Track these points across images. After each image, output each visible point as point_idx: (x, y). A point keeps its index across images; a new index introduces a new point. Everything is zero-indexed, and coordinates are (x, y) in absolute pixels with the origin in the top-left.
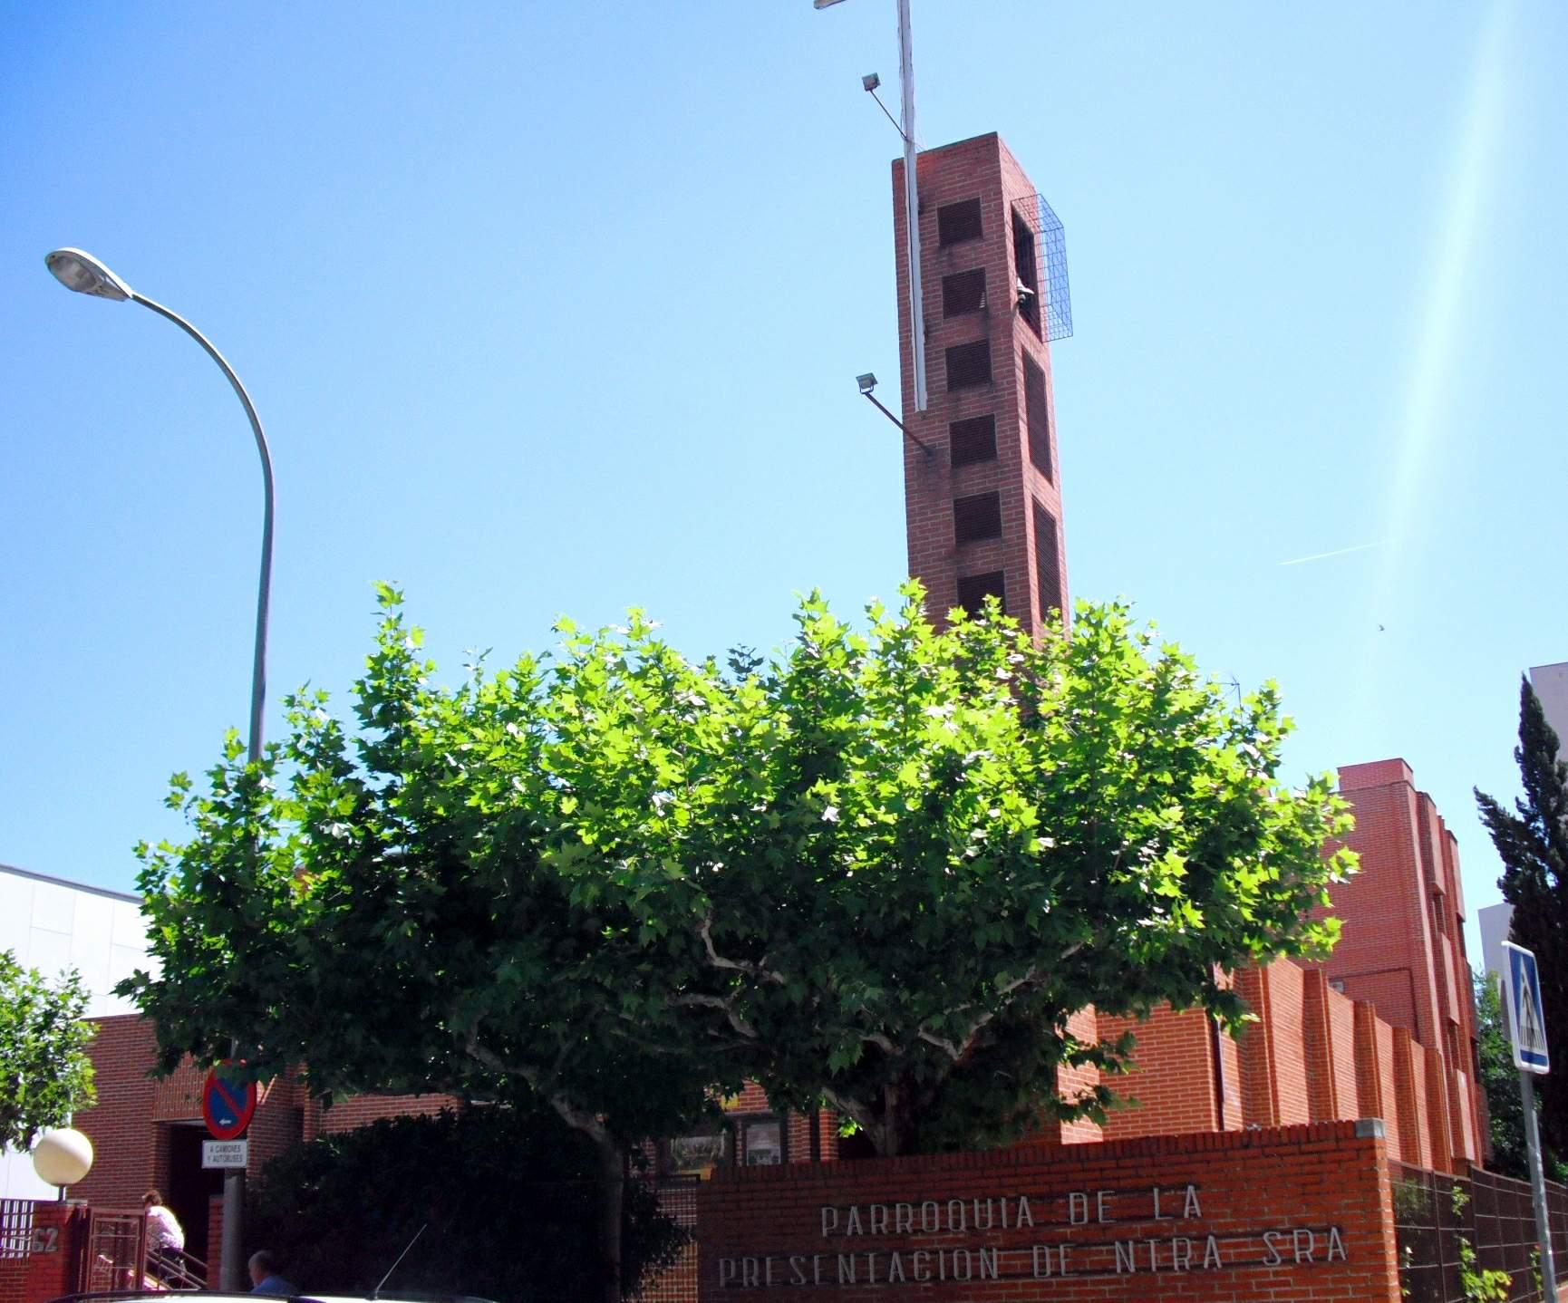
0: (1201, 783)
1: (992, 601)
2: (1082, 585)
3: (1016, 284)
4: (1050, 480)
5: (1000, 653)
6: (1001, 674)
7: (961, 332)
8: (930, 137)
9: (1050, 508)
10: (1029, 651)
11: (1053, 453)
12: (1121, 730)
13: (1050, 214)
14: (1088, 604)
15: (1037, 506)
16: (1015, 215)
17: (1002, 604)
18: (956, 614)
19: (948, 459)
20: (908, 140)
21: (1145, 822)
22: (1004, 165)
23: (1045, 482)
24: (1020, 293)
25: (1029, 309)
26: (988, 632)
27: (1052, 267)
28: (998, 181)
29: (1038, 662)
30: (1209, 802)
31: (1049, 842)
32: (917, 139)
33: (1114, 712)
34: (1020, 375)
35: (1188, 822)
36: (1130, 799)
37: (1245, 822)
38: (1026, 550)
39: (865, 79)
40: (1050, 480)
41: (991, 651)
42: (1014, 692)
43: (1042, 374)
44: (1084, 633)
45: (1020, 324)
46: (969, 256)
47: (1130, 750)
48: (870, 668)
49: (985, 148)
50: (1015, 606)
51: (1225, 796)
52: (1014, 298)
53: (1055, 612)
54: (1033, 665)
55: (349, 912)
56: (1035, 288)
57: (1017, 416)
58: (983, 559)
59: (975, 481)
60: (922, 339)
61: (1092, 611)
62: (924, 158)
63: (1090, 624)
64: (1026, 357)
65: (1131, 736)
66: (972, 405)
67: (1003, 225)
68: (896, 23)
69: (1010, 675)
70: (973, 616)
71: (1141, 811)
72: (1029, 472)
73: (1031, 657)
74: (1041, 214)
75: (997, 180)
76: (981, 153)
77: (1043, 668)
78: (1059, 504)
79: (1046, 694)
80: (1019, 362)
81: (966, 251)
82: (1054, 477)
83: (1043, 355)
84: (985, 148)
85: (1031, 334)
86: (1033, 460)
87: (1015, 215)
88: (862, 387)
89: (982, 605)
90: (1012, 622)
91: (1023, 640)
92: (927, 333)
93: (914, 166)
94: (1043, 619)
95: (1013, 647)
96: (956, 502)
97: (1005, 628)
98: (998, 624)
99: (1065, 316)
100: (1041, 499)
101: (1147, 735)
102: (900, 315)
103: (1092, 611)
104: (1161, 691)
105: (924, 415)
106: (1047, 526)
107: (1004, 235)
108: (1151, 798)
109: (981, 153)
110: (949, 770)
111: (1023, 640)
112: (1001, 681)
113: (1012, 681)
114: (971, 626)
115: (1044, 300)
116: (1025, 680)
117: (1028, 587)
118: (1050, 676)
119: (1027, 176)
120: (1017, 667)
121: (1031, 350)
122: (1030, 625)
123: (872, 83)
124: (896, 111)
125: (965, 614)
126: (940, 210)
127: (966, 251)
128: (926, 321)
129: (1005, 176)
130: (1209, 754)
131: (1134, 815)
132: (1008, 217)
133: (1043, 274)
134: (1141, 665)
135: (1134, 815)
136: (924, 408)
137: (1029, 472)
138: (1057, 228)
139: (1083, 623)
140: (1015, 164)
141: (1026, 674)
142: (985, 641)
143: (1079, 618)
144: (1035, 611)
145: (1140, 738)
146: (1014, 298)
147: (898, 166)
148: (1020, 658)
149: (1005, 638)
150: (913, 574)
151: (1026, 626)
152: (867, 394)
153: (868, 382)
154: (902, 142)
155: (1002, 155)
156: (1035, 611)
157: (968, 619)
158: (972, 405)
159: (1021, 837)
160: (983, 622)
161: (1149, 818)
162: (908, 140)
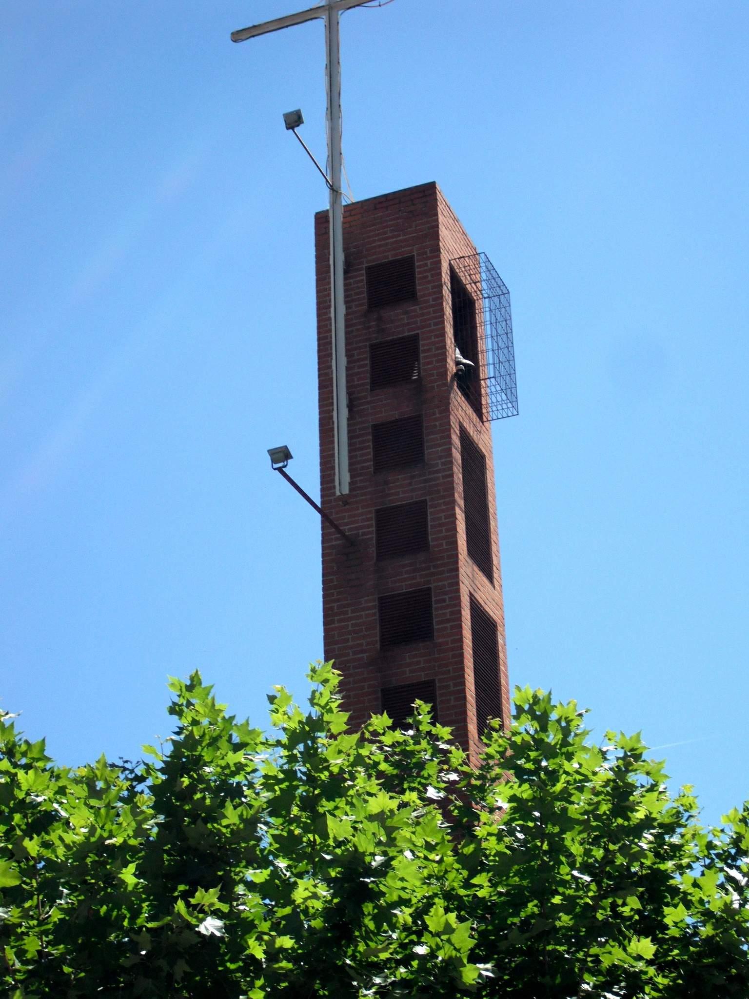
0: (675, 916)
1: (423, 708)
2: (522, 677)
3: (454, 354)
4: (490, 576)
5: (431, 769)
6: (432, 793)
7: (388, 407)
8: (356, 190)
9: (491, 610)
10: (465, 768)
11: (494, 548)
12: (574, 843)
13: (494, 277)
14: (530, 693)
15: (477, 610)
16: (454, 277)
17: (433, 709)
18: (380, 721)
19: (373, 550)
20: (335, 190)
21: (606, 962)
22: (443, 219)
23: (485, 580)
24: (458, 363)
25: (469, 382)
26: (417, 743)
27: (494, 324)
28: (436, 236)
29: (474, 782)
30: (685, 941)
31: (486, 969)
32: (344, 190)
33: (566, 822)
34: (457, 455)
35: (659, 962)
36: (593, 929)
37: (732, 962)
38: (462, 655)
39: (287, 117)
40: (490, 576)
41: (421, 765)
42: (447, 815)
43: (483, 457)
44: (526, 727)
45: (457, 399)
46: (399, 321)
47: (586, 868)
48: (266, 761)
49: (420, 202)
50: (449, 712)
51: (706, 931)
52: (452, 368)
53: (495, 723)
54: (469, 784)
55: (291, 970)
56: (475, 359)
57: (454, 502)
58: (412, 664)
59: (404, 577)
60: (344, 412)
61: (536, 700)
62: (353, 210)
63: (534, 717)
64: (465, 437)
65: (587, 853)
66: (402, 489)
67: (440, 286)
68: (323, 60)
69: (442, 794)
70: (399, 724)
71: (602, 945)
72: (467, 568)
73: (466, 776)
74: (484, 276)
75: (435, 235)
76: (419, 204)
77: (482, 789)
78: (500, 606)
79: (484, 816)
80: (456, 440)
81: (400, 321)
82: (495, 575)
83: (484, 437)
84: (420, 202)
85: (470, 411)
86: (471, 553)
87: (454, 277)
88: (274, 461)
89: (410, 712)
90: (445, 732)
91: (457, 756)
92: (351, 407)
93: (340, 219)
94: (480, 733)
95: (447, 762)
96: (381, 599)
97: (437, 738)
98: (429, 733)
99: (510, 391)
100: (480, 597)
101: (606, 850)
102: (321, 387)
103: (536, 700)
104: (621, 794)
105: (345, 500)
106: (486, 630)
107: (441, 297)
108: (615, 930)
109: (419, 204)
110: (355, 882)
111: (457, 756)
112: (431, 801)
113: (443, 804)
114: (398, 735)
115: (487, 371)
116: (459, 803)
117: (465, 698)
118: (489, 798)
119: (472, 230)
120: (451, 787)
121: (471, 431)
122: (467, 742)
123: (294, 121)
124: (322, 156)
125: (390, 722)
126: (368, 269)
127: (400, 321)
128: (350, 394)
129: (443, 232)
130: (681, 882)
131: (594, 950)
132: (446, 278)
133: (485, 344)
134: (593, 763)
135: (594, 950)
136: (346, 491)
137: (467, 568)
138: (501, 292)
139: (524, 717)
140: (455, 220)
141: (461, 796)
142: (412, 754)
143: (520, 709)
144: (472, 728)
145: (599, 853)
146: (452, 368)
147: (322, 220)
148: (454, 777)
149: (437, 751)
150: (327, 660)
151: (461, 739)
152: (280, 470)
153: (281, 456)
154: (327, 192)
155: (441, 207)
156: (472, 728)
157: (393, 728)
158: (402, 489)
159: (452, 965)
160: (411, 732)
161: (612, 955)
162: (335, 190)
